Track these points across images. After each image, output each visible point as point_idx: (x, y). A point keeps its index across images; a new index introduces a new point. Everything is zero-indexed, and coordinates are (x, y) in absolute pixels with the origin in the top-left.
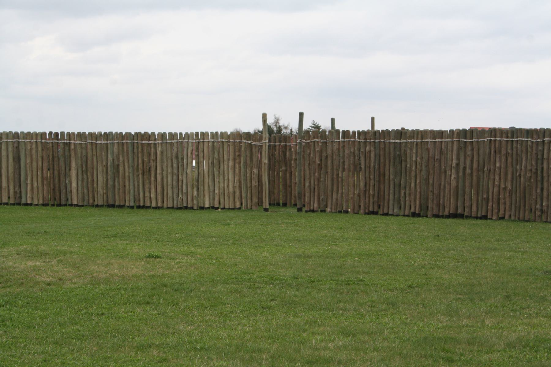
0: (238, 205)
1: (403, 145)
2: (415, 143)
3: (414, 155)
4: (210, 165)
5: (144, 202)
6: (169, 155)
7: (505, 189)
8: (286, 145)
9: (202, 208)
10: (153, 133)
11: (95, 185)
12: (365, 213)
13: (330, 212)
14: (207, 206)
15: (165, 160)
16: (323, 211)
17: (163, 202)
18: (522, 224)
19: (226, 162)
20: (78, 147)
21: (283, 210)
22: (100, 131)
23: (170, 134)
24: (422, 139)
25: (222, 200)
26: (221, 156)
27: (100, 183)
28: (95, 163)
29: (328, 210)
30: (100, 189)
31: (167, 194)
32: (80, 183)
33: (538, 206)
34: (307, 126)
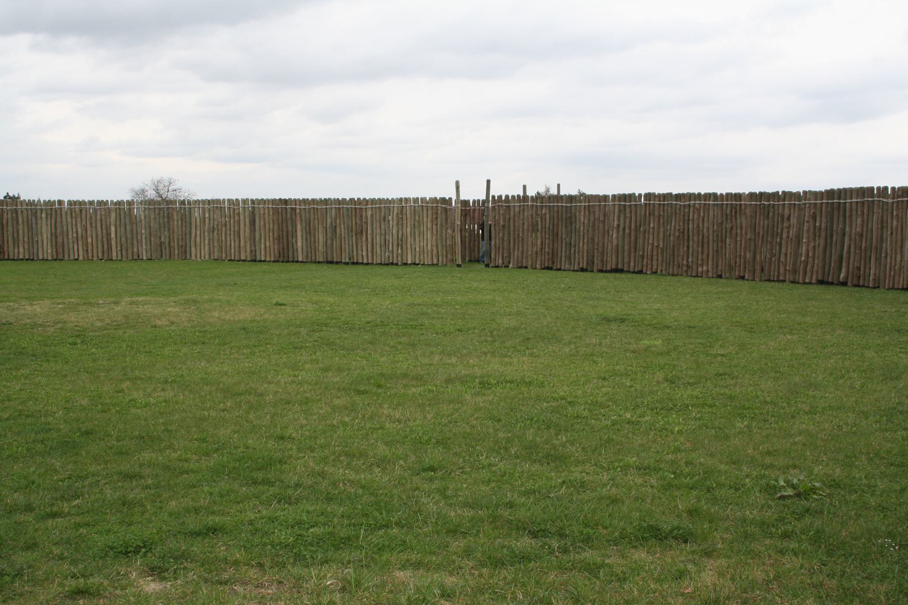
7: (658, 247)
9: (406, 264)
14: (409, 262)
30: (320, 248)
33: (685, 262)
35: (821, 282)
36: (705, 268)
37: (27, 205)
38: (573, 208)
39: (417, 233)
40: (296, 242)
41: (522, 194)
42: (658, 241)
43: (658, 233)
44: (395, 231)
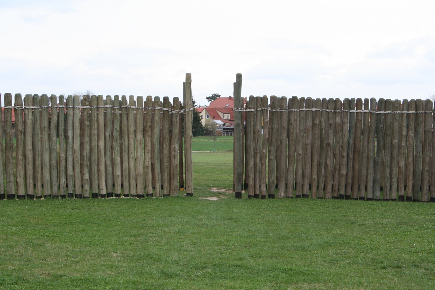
0: (410, 193)
1: (389, 117)
2: (405, 115)
3: (405, 129)
4: (108, 139)
5: (145, 187)
8: (408, 110)
9: (95, 196)
12: (334, 198)
13: (284, 197)
15: (38, 131)
19: (132, 135)
24: (416, 110)
26: (124, 128)
34: (245, 94)
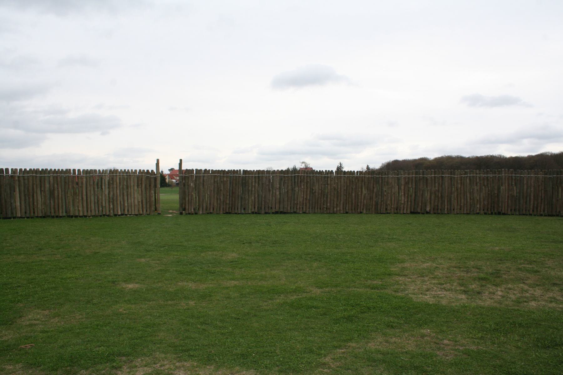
6: (92, 183)
7: (306, 199)
9: (115, 215)
10: (354, 171)
11: (35, 204)
14: (120, 213)
16: (196, 214)
17: (34, 213)
18: (378, 215)
19: (132, 187)
20: (21, 179)
21: (335, 215)
22: (68, 168)
23: (196, 170)
25: (130, 210)
26: (129, 184)
27: (40, 202)
28: (35, 189)
29: (365, 212)
30: (39, 206)
31: (91, 207)
32: (23, 202)
33: (325, 206)
35: (412, 213)
36: (338, 209)
37: (120, 173)
38: (247, 178)
39: (125, 194)
40: (15, 202)
41: (177, 168)
42: (306, 196)
43: (307, 192)
44: (107, 193)
